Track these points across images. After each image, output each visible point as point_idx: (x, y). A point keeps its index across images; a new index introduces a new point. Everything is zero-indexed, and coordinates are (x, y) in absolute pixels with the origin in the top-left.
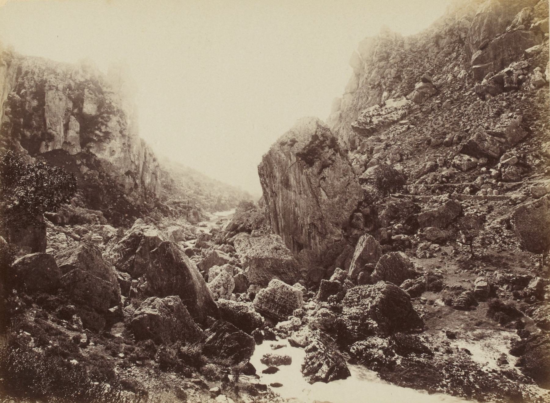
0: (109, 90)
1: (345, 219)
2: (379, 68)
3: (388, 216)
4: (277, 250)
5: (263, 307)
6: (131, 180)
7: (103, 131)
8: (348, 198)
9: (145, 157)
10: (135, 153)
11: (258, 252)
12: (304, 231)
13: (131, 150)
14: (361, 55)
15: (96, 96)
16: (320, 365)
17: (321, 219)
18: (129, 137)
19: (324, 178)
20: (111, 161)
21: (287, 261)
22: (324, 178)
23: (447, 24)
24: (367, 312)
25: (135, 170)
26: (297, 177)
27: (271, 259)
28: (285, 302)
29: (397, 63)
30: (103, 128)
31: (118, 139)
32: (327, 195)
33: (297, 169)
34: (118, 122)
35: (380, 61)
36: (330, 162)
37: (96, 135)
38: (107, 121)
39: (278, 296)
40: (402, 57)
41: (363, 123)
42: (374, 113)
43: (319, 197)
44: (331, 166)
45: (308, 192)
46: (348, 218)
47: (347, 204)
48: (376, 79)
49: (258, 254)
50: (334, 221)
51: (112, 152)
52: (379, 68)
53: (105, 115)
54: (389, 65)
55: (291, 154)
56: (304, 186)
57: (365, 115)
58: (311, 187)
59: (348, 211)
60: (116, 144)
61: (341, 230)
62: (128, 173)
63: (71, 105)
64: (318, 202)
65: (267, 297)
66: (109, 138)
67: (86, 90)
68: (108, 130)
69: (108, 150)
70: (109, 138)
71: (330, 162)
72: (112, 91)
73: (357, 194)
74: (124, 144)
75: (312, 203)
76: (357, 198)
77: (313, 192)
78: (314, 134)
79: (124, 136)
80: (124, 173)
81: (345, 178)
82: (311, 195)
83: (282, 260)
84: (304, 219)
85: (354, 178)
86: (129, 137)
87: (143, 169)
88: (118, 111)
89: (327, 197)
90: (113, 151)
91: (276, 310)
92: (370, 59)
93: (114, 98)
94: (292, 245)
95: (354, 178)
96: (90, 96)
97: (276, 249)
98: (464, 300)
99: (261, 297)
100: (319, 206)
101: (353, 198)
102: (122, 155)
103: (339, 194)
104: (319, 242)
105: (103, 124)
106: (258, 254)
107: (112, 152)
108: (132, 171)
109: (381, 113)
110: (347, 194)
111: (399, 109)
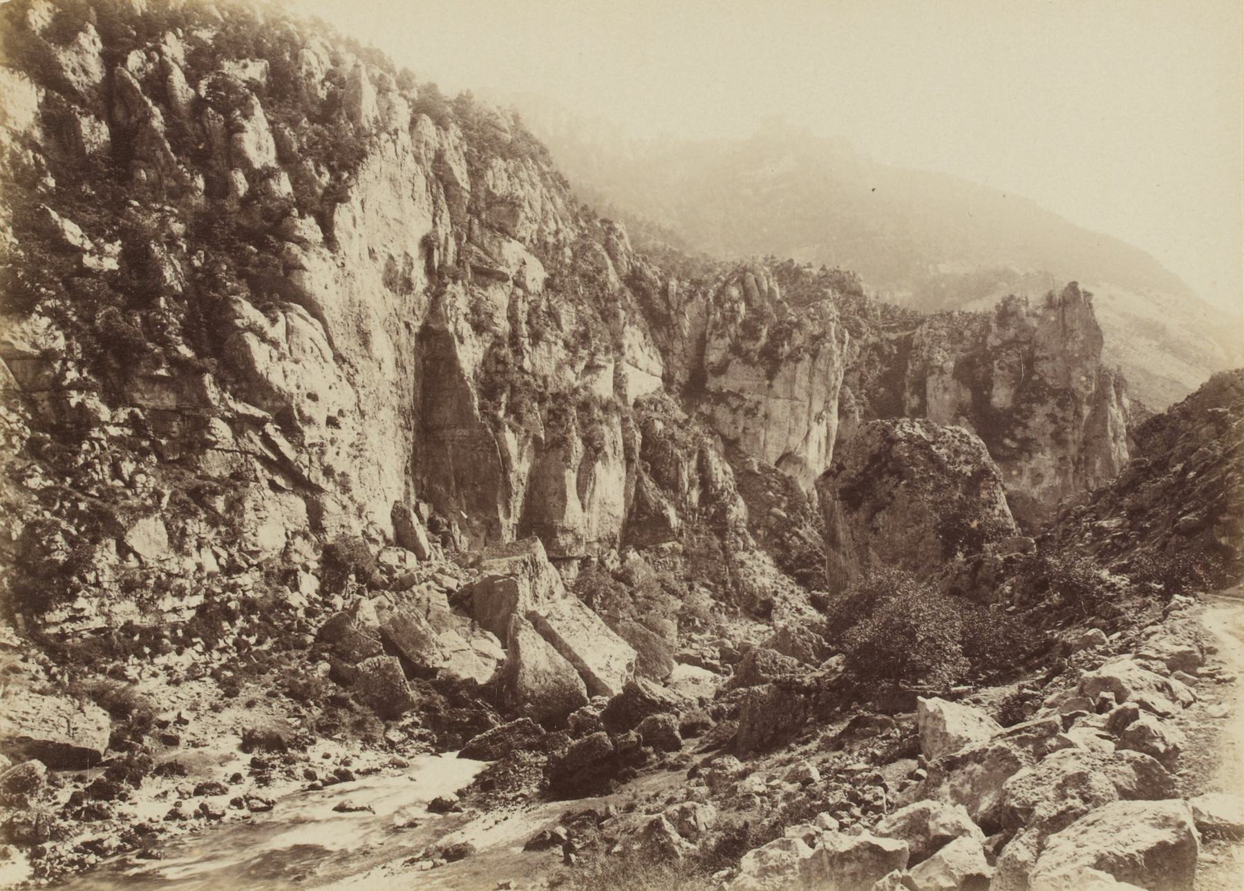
7: (1019, 437)
20: (1035, 496)
22: (875, 530)
30: (1019, 432)
31: (1048, 451)
36: (889, 499)
38: (1026, 417)
51: (1037, 477)
69: (1027, 473)
81: (916, 528)
102: (1058, 481)
105: (1018, 424)
107: (1037, 477)
110: (919, 557)
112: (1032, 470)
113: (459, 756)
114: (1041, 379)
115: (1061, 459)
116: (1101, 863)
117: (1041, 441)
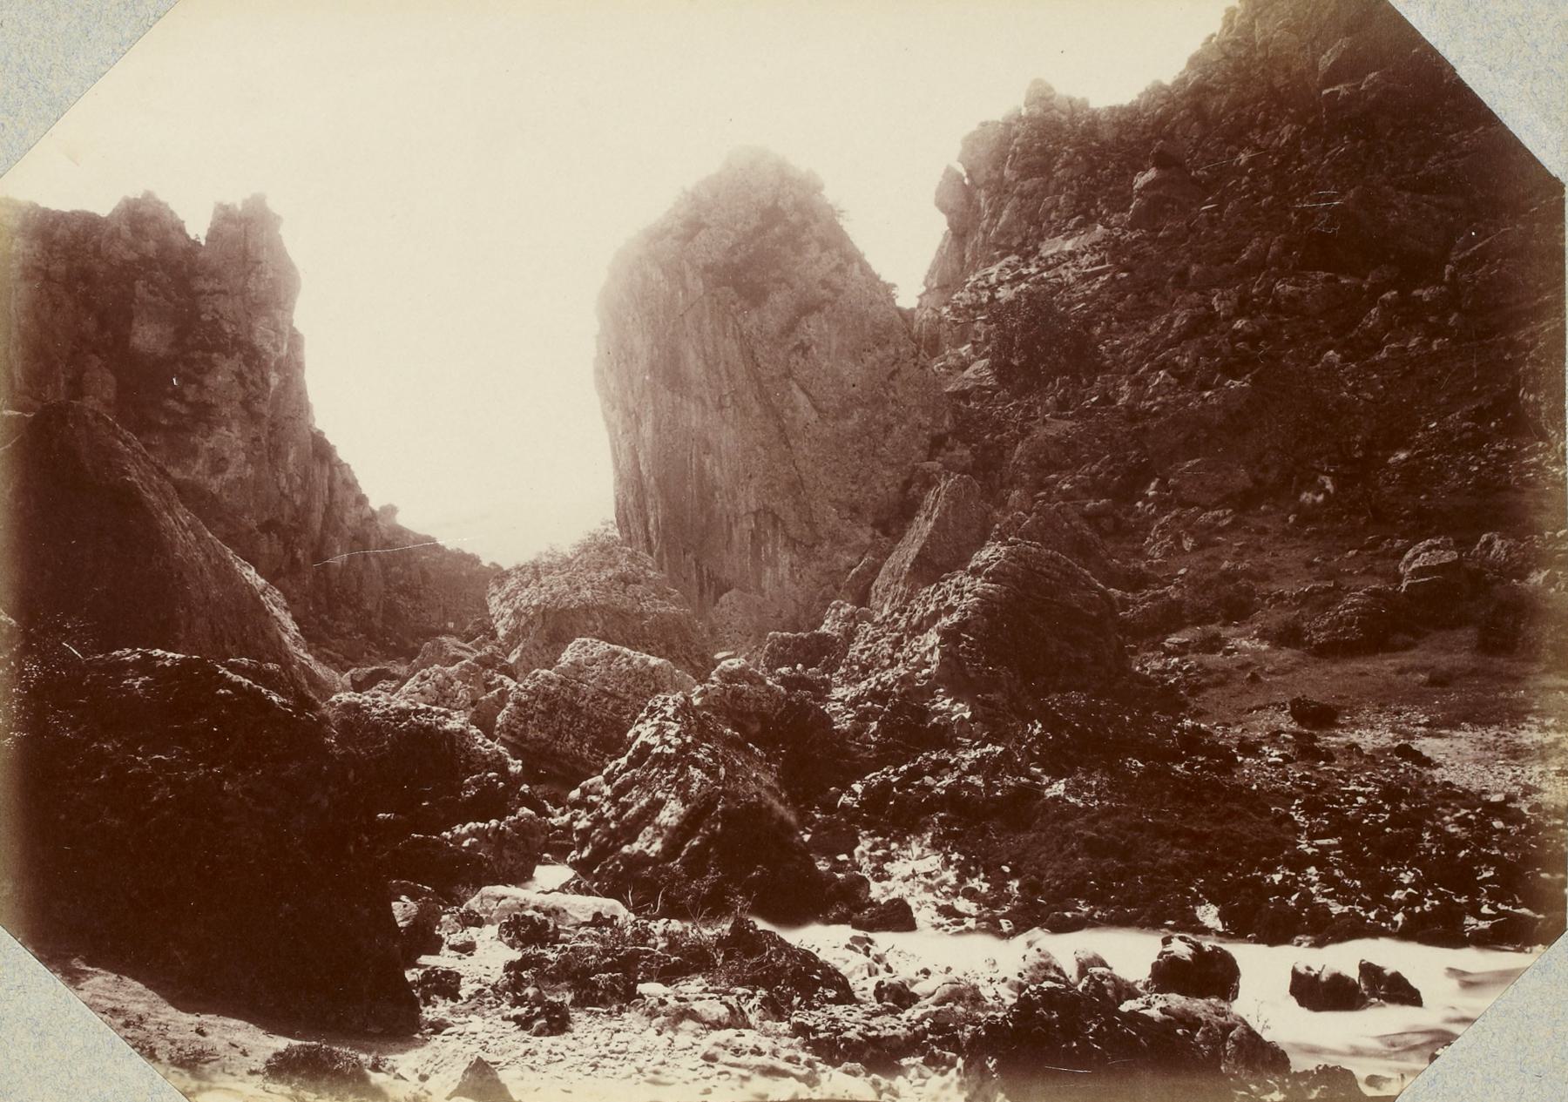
0: (208, 286)
1: (881, 490)
2: (1021, 195)
3: (1036, 459)
4: (627, 583)
5: (531, 735)
6: (278, 548)
7: (190, 398)
8: (893, 420)
9: (331, 490)
10: (291, 468)
16: (657, 805)
19: (803, 349)
21: (661, 615)
23: (1227, 57)
24: (928, 677)
25: (293, 519)
26: (709, 350)
28: (616, 709)
29: (1078, 178)
32: (815, 407)
33: (707, 321)
34: (240, 375)
35: (1024, 177)
37: (169, 413)
38: (201, 371)
40: (1091, 160)
41: (968, 307)
44: (828, 308)
45: (749, 396)
46: (893, 489)
47: (889, 443)
48: (1015, 229)
49: (554, 596)
50: (842, 497)
52: (1021, 195)
53: (197, 355)
56: (731, 377)
57: (975, 286)
58: (758, 379)
59: (892, 464)
60: (231, 438)
61: (869, 530)
62: (268, 527)
63: (90, 324)
64: (782, 429)
65: (546, 697)
66: (208, 422)
67: (139, 285)
70: (208, 422)
71: (826, 293)
74: (256, 439)
75: (761, 435)
76: (927, 421)
77: (763, 396)
79: (255, 418)
80: (254, 524)
82: (757, 410)
83: (641, 615)
84: (735, 496)
85: (915, 355)
87: (325, 524)
88: (237, 343)
89: (814, 416)
91: (581, 739)
92: (995, 176)
93: (226, 306)
94: (696, 590)
96: (154, 299)
97: (624, 580)
99: (525, 698)
101: (910, 420)
103: (861, 405)
106: (554, 596)
108: (285, 522)
109: (1025, 272)
111: (1083, 254)
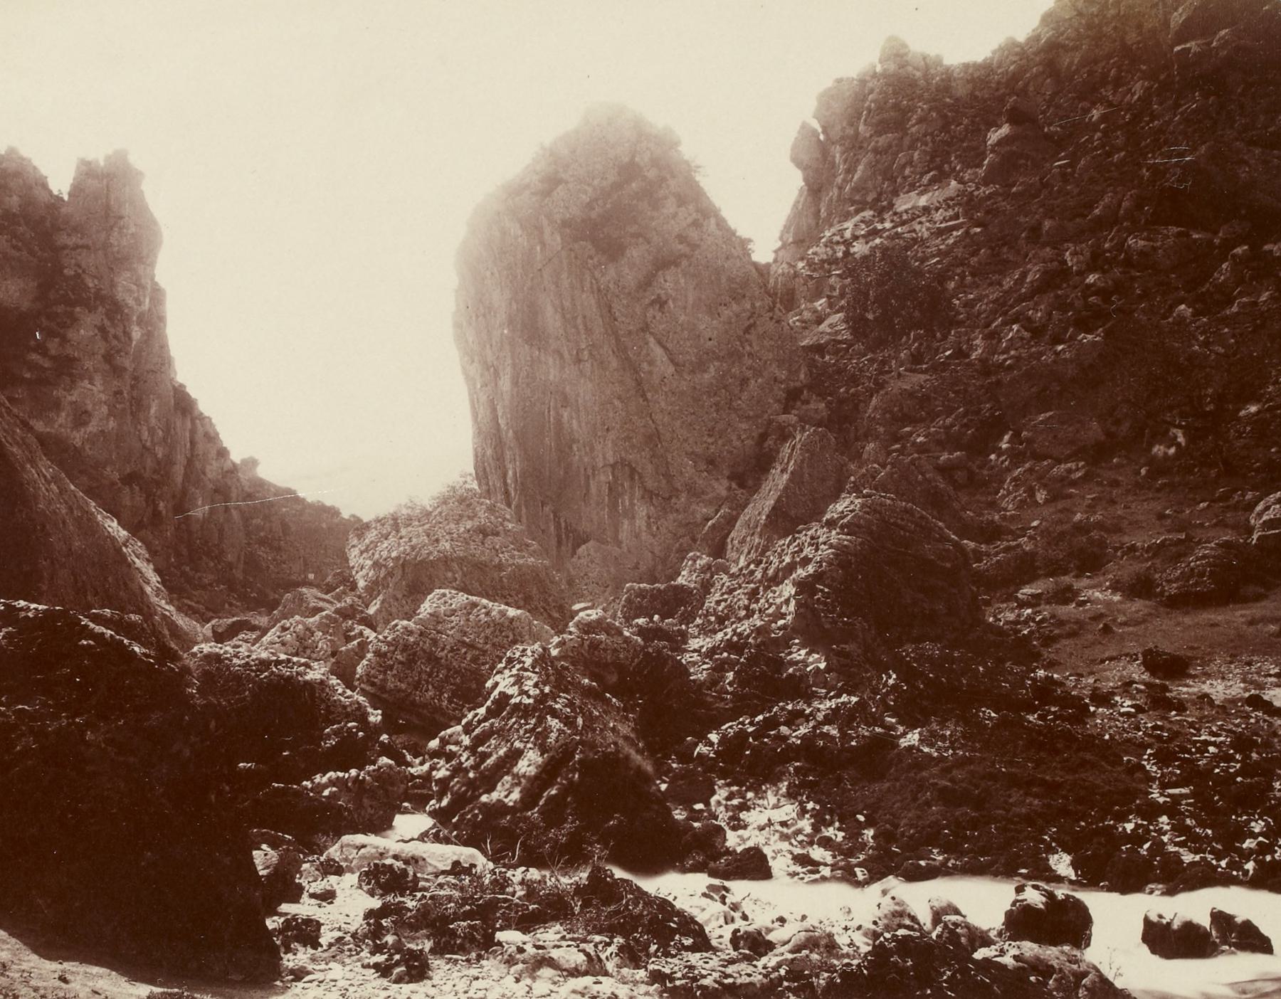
2: (876, 151)
3: (891, 412)
4: (485, 535)
6: (140, 499)
7: (53, 352)
8: (749, 373)
10: (153, 421)
11: (414, 541)
12: (593, 490)
13: (141, 416)
14: (825, 132)
15: (32, 253)
16: (515, 755)
17: (653, 439)
18: (136, 378)
19: (661, 303)
20: (78, 442)
21: (519, 567)
23: (1080, 14)
24: (784, 627)
26: (567, 304)
27: (461, 560)
28: (475, 660)
32: (672, 361)
34: (102, 329)
35: (879, 133)
37: (33, 367)
38: (64, 326)
39: (447, 639)
41: (823, 261)
42: (857, 233)
43: (645, 366)
44: (685, 263)
46: (749, 442)
47: (745, 396)
48: (870, 184)
49: (413, 548)
50: (699, 450)
52: (876, 151)
53: (60, 309)
54: (907, 141)
55: (545, 222)
56: (589, 331)
57: (831, 241)
58: (615, 333)
59: (748, 418)
60: (93, 391)
61: (726, 483)
64: (639, 383)
65: (406, 647)
66: (71, 375)
68: (69, 351)
70: (71, 375)
71: (683, 248)
72: (81, 242)
73: (781, 362)
74: (118, 393)
76: (783, 375)
77: (620, 350)
78: (627, 159)
79: (117, 371)
81: (735, 307)
82: (614, 363)
83: (500, 567)
84: (592, 449)
85: (771, 309)
86: (136, 378)
88: (100, 297)
89: (671, 369)
90: (86, 412)
92: (850, 131)
93: (89, 261)
95: (771, 309)
96: (15, 253)
97: (483, 532)
98: (1209, 564)
99: (384, 648)
100: (643, 395)
103: (718, 358)
104: (649, 526)
106: (413, 548)
108: (147, 475)
109: (880, 227)
111: (937, 209)
112: (72, 403)
113: (1163, 894)
114: (78, 276)
115: (116, 393)
116: (574, 992)
117: (88, 364)
